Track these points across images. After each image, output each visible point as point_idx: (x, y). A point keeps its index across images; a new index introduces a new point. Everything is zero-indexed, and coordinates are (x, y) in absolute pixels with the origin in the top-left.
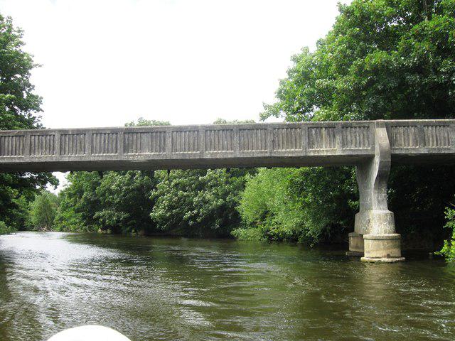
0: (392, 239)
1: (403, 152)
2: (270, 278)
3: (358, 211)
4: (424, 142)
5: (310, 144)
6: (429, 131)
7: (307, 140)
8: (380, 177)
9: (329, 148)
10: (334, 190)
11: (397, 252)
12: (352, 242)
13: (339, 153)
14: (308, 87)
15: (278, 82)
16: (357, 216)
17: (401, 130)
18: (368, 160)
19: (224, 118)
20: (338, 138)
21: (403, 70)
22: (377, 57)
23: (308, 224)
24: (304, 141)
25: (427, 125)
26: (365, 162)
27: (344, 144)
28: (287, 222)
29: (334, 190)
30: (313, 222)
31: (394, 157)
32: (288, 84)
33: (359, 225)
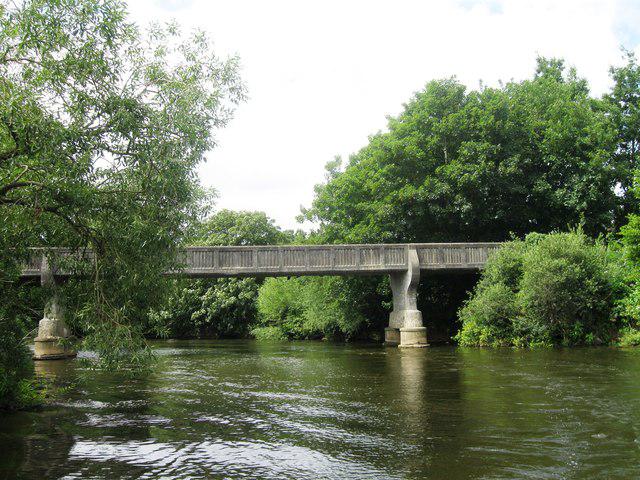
0: (420, 331)
1: (428, 267)
2: (304, 389)
3: (391, 310)
4: (443, 260)
5: (362, 262)
6: (447, 252)
7: (105, 152)
8: (412, 285)
9: (374, 264)
10: (370, 300)
11: (424, 340)
12: (389, 336)
13: (382, 268)
14: (346, 203)
15: (536, 65)
16: (391, 314)
17: (427, 251)
18: (403, 273)
19: (271, 215)
20: (382, 257)
21: (426, 203)
22: (408, 191)
23: (341, 322)
24: (358, 259)
25: (445, 247)
26: (399, 275)
27: (386, 261)
28: (313, 320)
29: (370, 300)
30: (347, 318)
31: (423, 271)
32: (561, 115)
33: (393, 321)
